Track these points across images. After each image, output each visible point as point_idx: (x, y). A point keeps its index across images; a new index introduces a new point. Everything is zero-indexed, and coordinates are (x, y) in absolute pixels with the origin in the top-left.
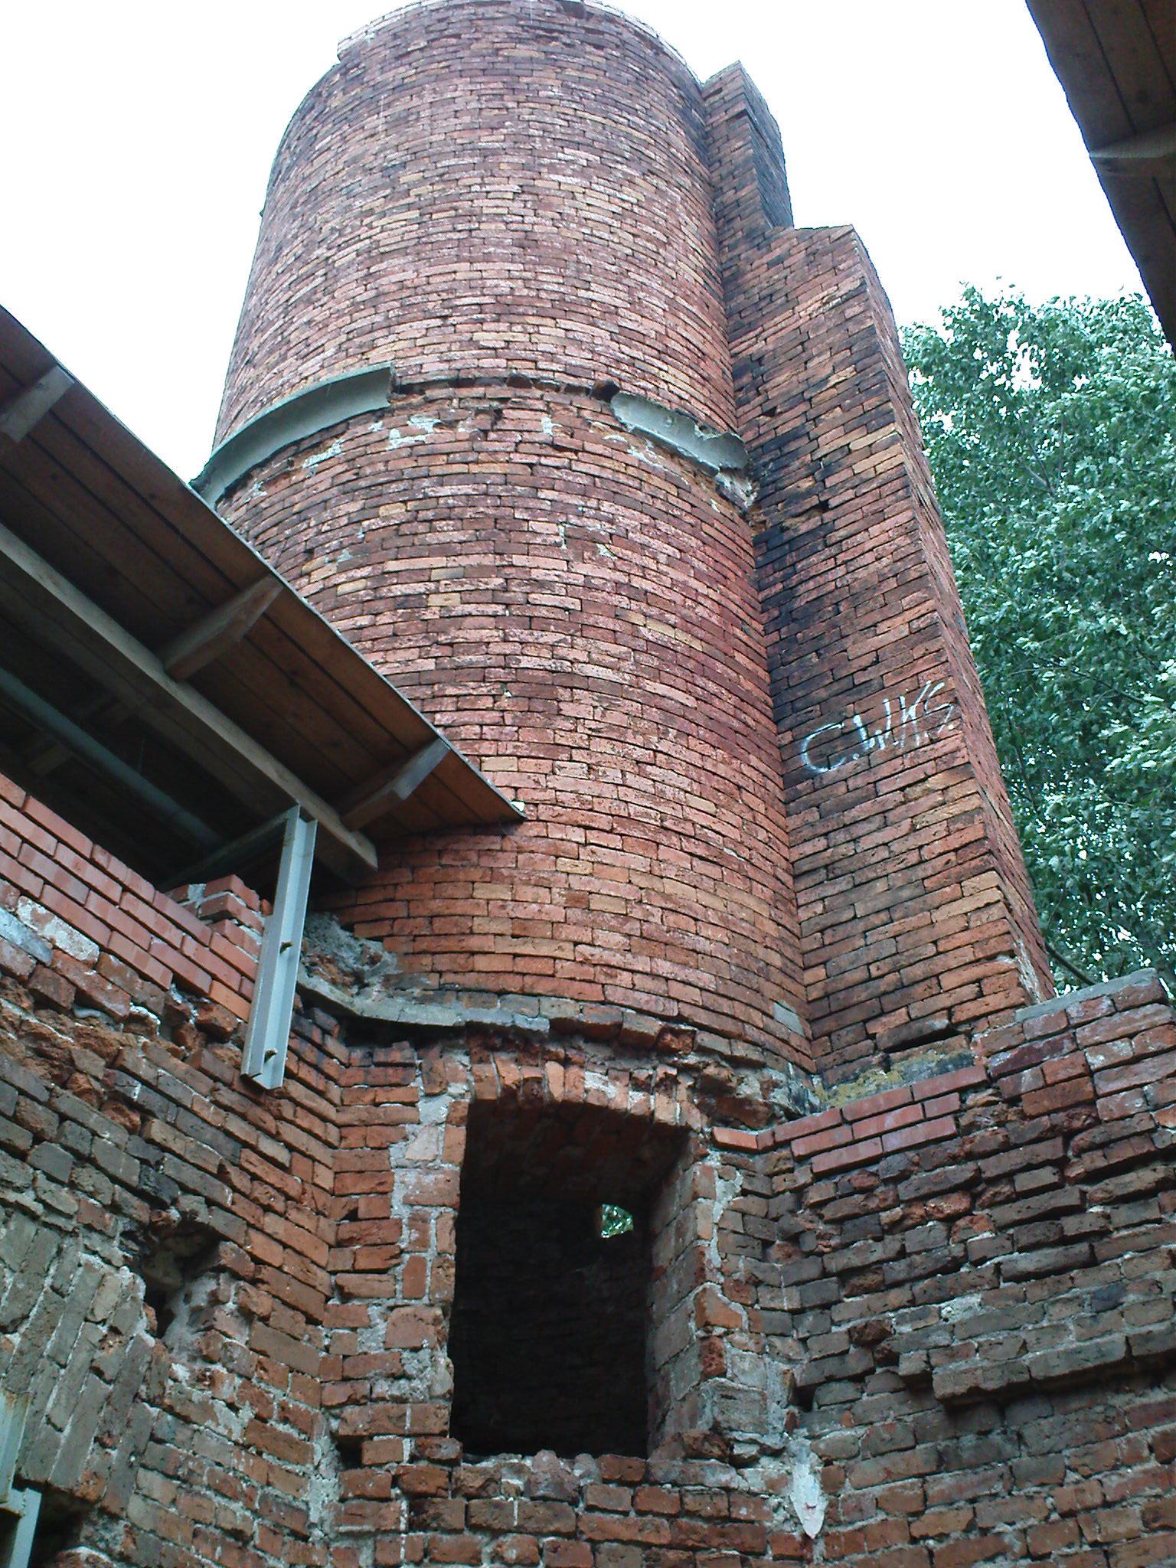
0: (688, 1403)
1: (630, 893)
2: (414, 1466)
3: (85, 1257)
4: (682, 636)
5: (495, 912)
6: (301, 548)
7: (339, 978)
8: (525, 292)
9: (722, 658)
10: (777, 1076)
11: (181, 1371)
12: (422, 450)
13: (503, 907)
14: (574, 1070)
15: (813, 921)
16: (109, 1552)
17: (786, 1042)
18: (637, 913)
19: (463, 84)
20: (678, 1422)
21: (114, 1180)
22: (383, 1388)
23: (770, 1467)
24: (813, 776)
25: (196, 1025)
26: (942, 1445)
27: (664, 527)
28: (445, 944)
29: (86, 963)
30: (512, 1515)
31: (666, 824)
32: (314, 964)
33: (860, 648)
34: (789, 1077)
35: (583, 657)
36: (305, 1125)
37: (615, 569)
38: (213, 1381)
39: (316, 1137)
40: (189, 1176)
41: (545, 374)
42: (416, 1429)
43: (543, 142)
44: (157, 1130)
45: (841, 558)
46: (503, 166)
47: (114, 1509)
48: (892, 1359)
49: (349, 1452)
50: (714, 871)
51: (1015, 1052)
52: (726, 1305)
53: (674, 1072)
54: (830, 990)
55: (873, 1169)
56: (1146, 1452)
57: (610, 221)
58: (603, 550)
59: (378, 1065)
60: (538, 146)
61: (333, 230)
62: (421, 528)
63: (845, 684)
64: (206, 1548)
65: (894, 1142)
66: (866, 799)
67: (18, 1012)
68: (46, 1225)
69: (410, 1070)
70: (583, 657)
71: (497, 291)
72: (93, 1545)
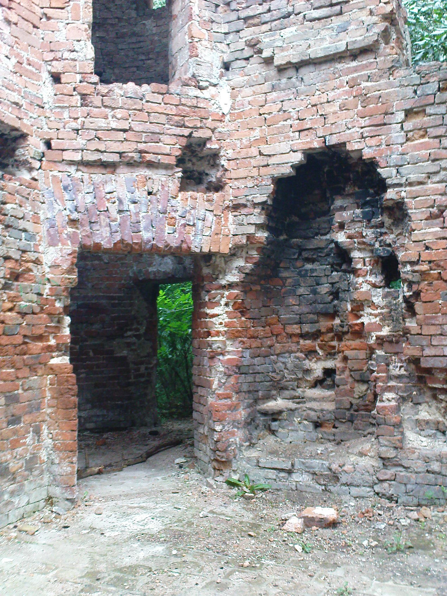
0: (183, 65)
2: (81, 84)
20: (180, 74)
22: (66, 55)
23: (212, 90)
26: (274, 82)
42: (81, 71)
48: (260, 51)
49: (56, 78)
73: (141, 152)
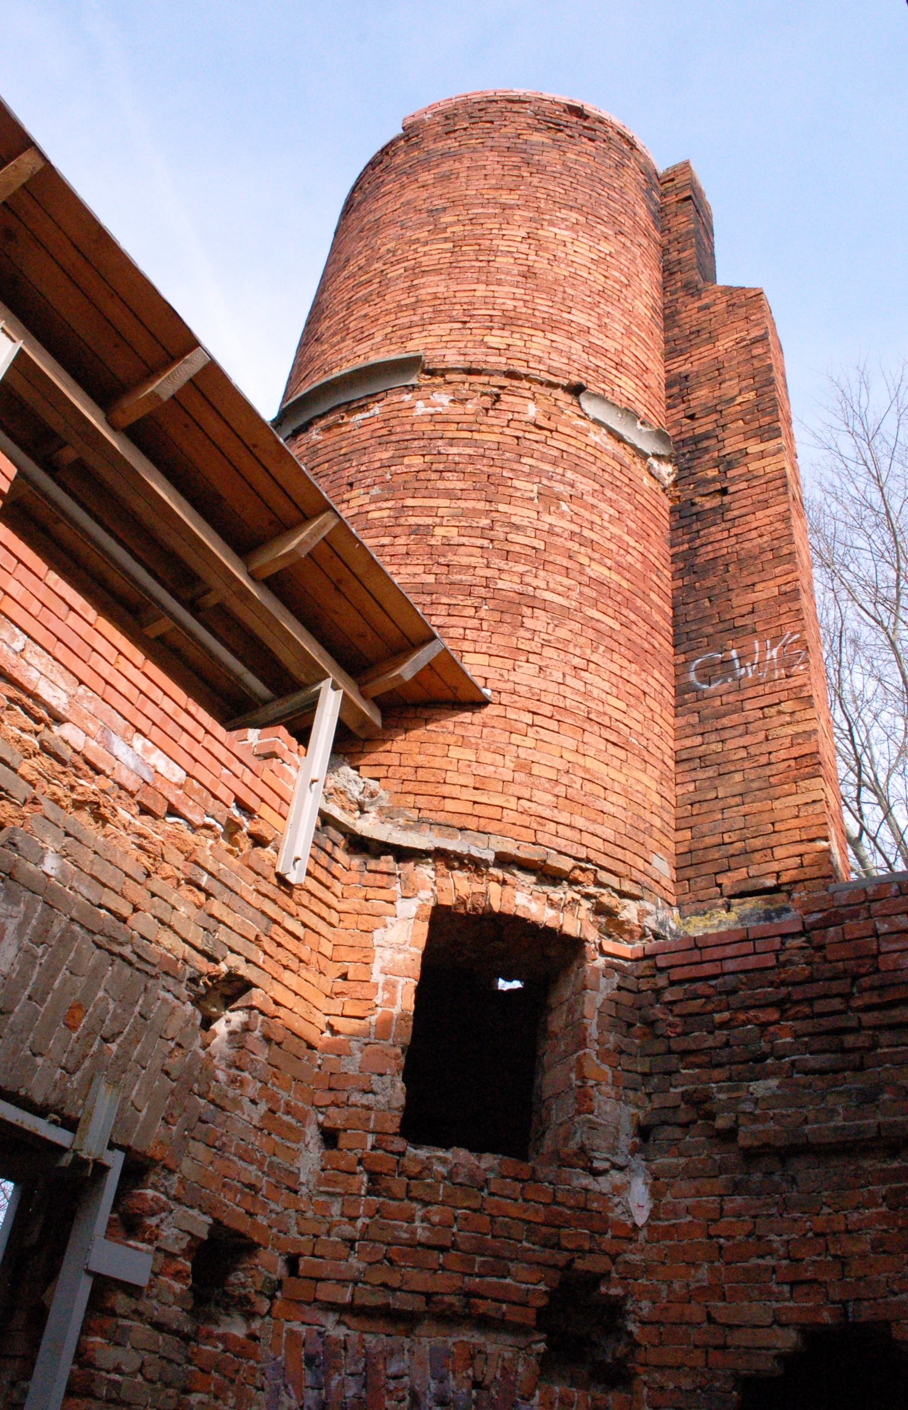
1: (561, 765)
3: (163, 994)
4: (615, 577)
5: (463, 769)
6: (345, 481)
7: (348, 806)
8: (524, 310)
9: (641, 595)
10: (648, 906)
11: (221, 1076)
12: (439, 418)
13: (469, 766)
14: (508, 889)
15: (686, 796)
16: (166, 1194)
17: (658, 882)
18: (565, 780)
19: (493, 157)
21: (185, 941)
22: (357, 1098)
23: (617, 1177)
24: (697, 690)
25: (246, 829)
27: (609, 493)
28: (424, 788)
29: (176, 784)
30: (438, 1193)
31: (591, 716)
32: (331, 794)
33: (741, 601)
34: (657, 908)
35: (543, 585)
36: (316, 910)
37: (572, 521)
38: (242, 1084)
39: (323, 919)
40: (237, 943)
41: (534, 372)
42: (378, 1129)
43: (547, 204)
44: (216, 908)
45: (734, 531)
46: (516, 218)
47: (172, 1166)
48: (712, 1116)
50: (621, 754)
51: (825, 914)
52: (598, 1065)
53: (578, 897)
54: (692, 848)
55: (713, 983)
56: (880, 1200)
57: (589, 265)
58: (564, 507)
59: (370, 871)
60: (542, 205)
61: (389, 251)
62: (434, 476)
63: (726, 625)
64: (230, 1195)
65: (730, 966)
66: (734, 712)
67: (128, 817)
68: (138, 970)
69: (392, 878)
70: (543, 585)
71: (504, 307)
72: (155, 1187)
73: (469, 1294)
